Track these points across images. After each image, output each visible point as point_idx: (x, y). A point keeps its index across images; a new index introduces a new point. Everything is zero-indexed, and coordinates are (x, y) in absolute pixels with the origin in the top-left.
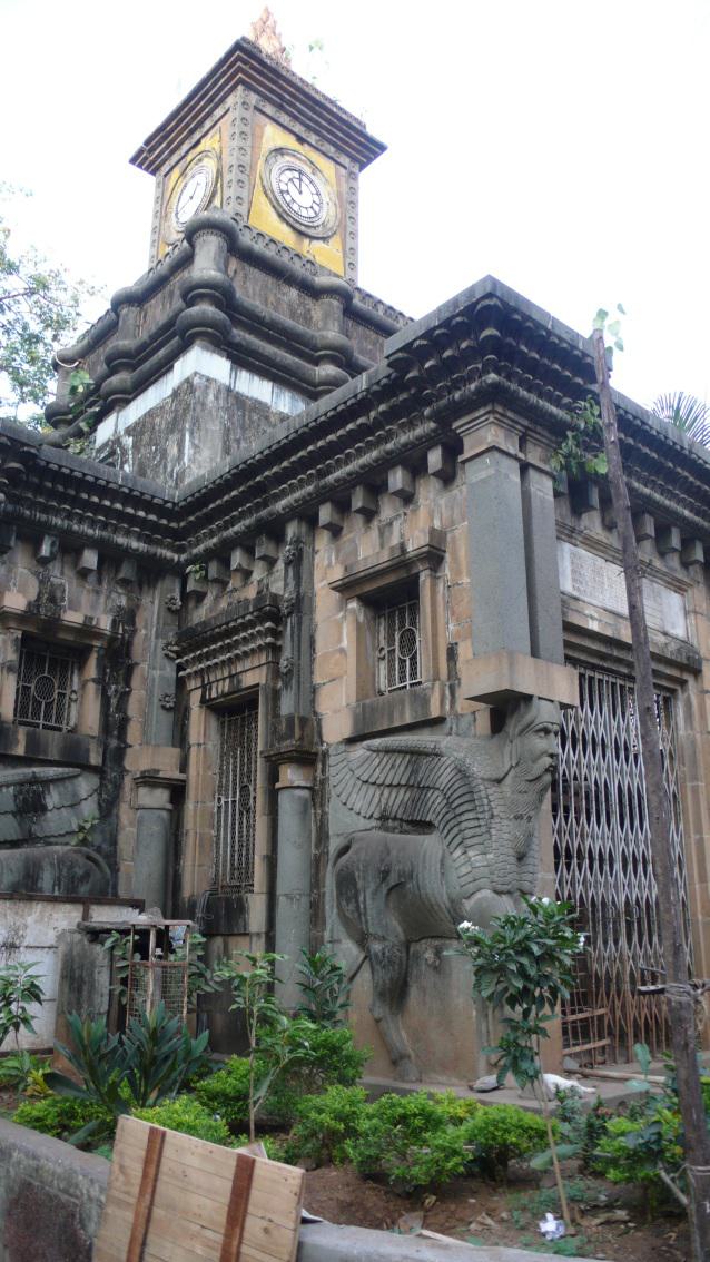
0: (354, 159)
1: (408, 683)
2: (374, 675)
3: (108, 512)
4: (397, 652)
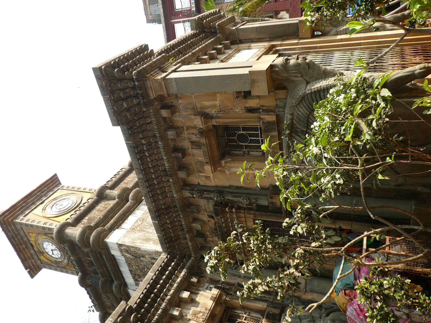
0: (57, 186)
1: (260, 139)
2: (255, 157)
3: (165, 282)
4: (246, 144)
